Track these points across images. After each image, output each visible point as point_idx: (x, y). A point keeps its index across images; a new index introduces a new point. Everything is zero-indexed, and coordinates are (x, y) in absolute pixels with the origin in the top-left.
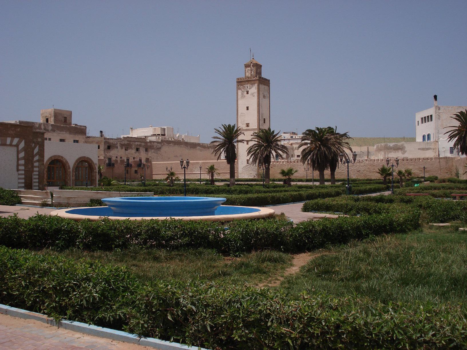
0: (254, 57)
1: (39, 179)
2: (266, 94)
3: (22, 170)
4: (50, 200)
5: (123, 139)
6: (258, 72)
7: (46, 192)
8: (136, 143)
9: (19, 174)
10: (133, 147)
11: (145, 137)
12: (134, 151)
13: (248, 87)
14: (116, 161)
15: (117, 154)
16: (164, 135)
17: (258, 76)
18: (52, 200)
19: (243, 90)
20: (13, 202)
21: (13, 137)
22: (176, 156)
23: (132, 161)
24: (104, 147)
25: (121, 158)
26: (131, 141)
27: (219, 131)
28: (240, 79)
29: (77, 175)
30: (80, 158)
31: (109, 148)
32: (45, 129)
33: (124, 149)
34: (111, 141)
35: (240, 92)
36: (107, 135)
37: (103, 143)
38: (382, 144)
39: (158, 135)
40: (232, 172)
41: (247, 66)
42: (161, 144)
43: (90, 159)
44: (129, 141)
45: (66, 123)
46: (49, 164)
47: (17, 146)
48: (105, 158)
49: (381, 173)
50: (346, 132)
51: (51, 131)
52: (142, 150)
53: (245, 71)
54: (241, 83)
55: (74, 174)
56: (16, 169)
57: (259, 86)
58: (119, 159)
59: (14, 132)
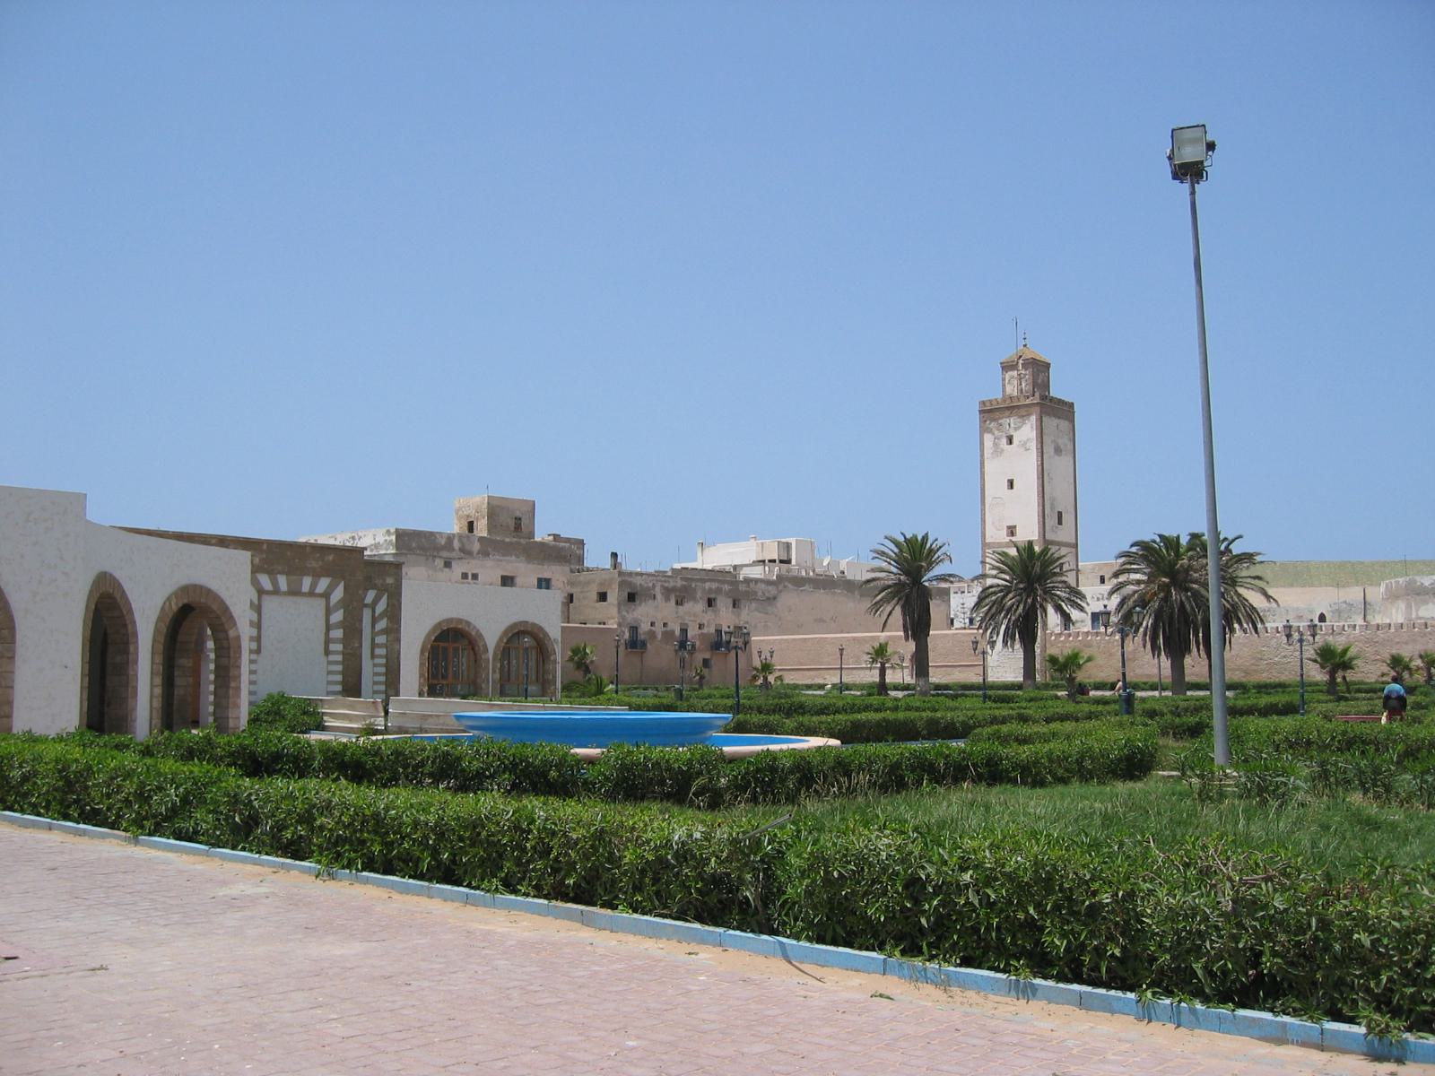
0: (1026, 336)
1: (386, 674)
2: (1064, 441)
3: (337, 653)
4: (381, 721)
5: (670, 574)
6: (1040, 381)
7: (373, 702)
8: (707, 585)
9: (329, 663)
10: (699, 594)
11: (735, 567)
12: (700, 606)
13: (1012, 425)
14: (652, 634)
15: (655, 615)
16: (788, 562)
17: (1037, 395)
18: (386, 720)
19: (996, 432)
20: (304, 724)
21: (317, 575)
22: (822, 620)
23: (694, 633)
24: (619, 596)
25: (665, 625)
26: (692, 580)
27: (883, 553)
28: (988, 404)
29: (506, 669)
30: (515, 625)
31: (632, 597)
32: (462, 550)
33: (673, 602)
34: (638, 581)
35: (988, 440)
36: (629, 565)
37: (615, 586)
38: (1401, 580)
39: (770, 561)
40: (921, 664)
41: (1007, 367)
42: (778, 588)
43: (541, 629)
44: (686, 579)
45: (519, 534)
46: (435, 641)
47: (326, 595)
48: (620, 625)
49: (1319, 660)
50: (1258, 551)
51: (478, 553)
52: (723, 604)
53: (1004, 380)
54: (991, 413)
55: (499, 665)
56: (369, 656)
57: (1040, 421)
58: (659, 629)
59: (320, 563)
